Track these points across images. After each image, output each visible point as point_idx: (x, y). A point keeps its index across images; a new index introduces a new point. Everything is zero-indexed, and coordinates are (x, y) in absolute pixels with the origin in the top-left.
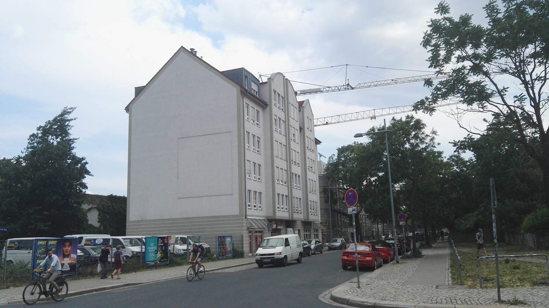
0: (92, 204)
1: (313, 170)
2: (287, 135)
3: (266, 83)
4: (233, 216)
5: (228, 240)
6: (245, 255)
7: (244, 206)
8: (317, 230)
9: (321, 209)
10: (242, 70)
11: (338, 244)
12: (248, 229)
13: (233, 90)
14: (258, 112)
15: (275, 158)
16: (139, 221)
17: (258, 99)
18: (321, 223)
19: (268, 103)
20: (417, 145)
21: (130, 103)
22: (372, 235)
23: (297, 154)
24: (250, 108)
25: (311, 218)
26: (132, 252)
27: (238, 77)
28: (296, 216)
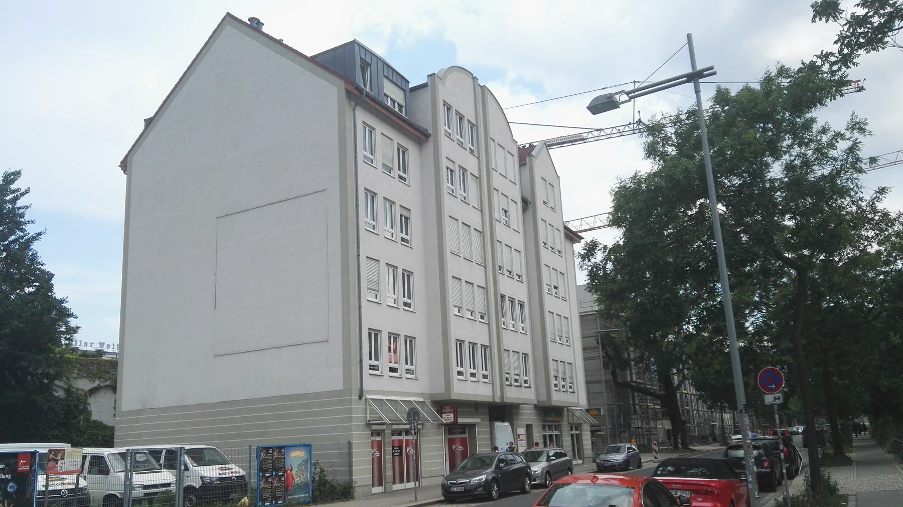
0: (99, 378)
1: (561, 294)
2: (485, 208)
3: (424, 86)
4: (331, 394)
5: (296, 457)
6: (358, 492)
7: (353, 367)
8: (578, 427)
9: (588, 383)
10: (352, 47)
11: (619, 458)
12: (369, 425)
13: (330, 91)
14: (403, 152)
15: (449, 257)
16: (139, 412)
17: (373, 99)
18: (588, 411)
19: (430, 131)
20: (807, 164)
21: (130, 152)
22: (712, 434)
23: (515, 254)
24: (378, 138)
25: (558, 398)
26: (202, 478)
27: (351, 70)
28: (513, 395)
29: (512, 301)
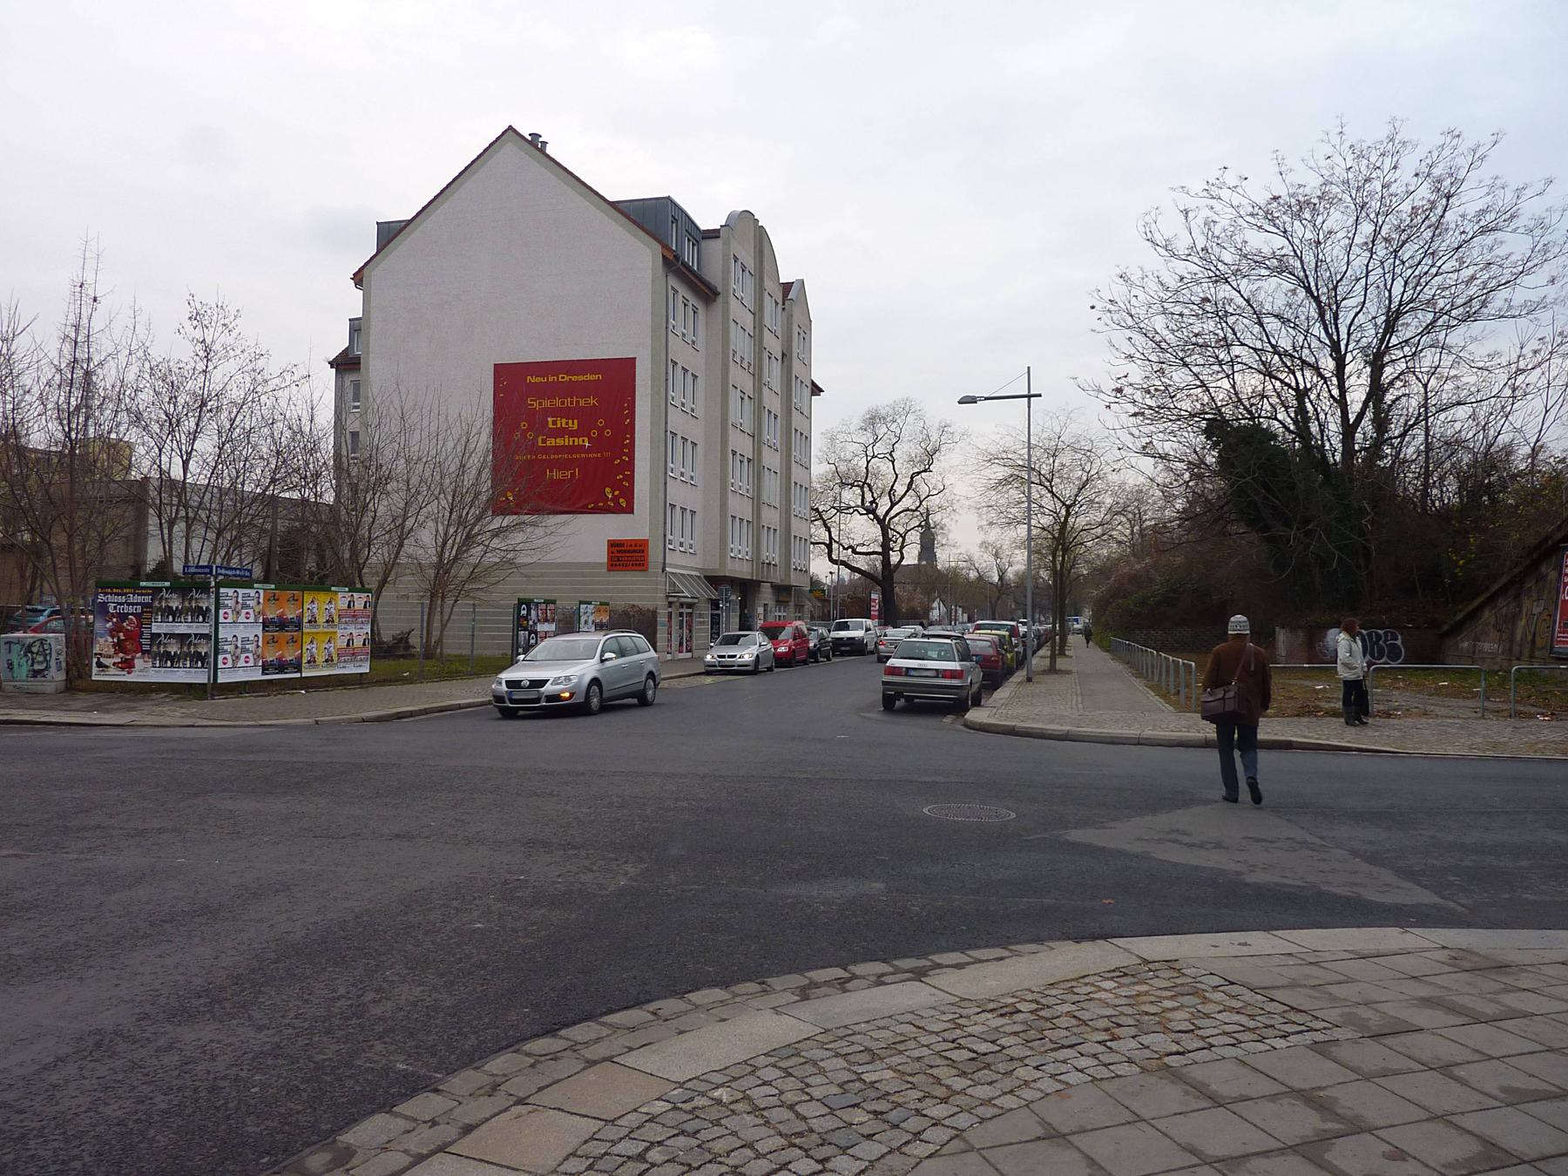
13: (644, 256)
27: (656, 219)
29: (684, 510)
